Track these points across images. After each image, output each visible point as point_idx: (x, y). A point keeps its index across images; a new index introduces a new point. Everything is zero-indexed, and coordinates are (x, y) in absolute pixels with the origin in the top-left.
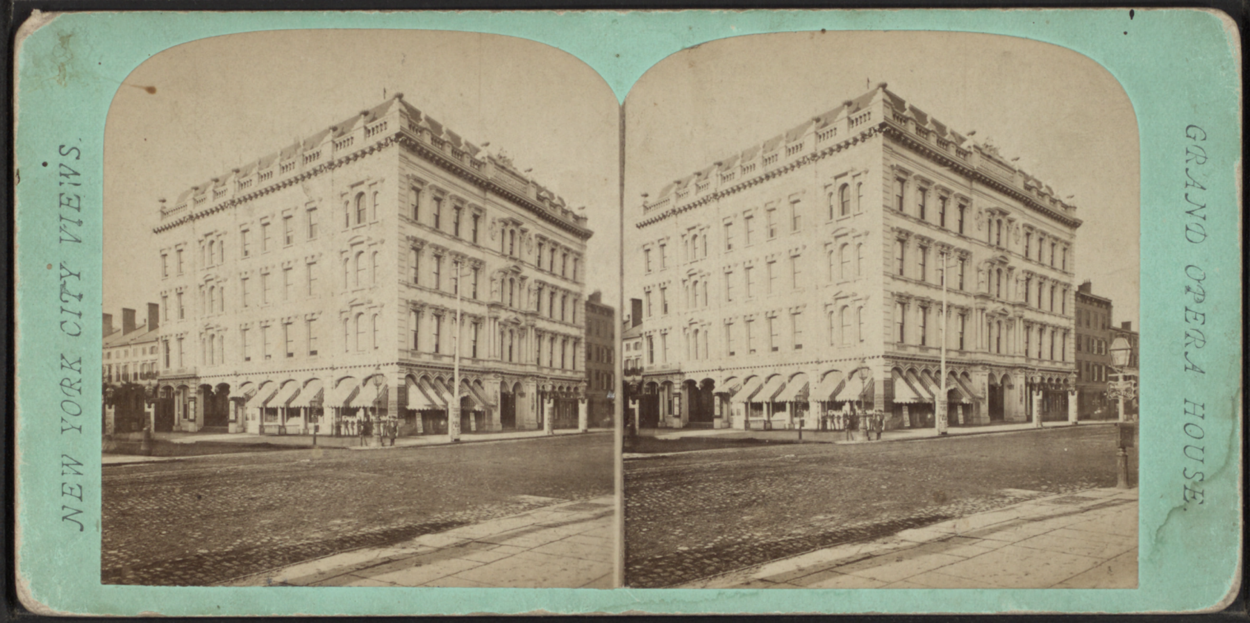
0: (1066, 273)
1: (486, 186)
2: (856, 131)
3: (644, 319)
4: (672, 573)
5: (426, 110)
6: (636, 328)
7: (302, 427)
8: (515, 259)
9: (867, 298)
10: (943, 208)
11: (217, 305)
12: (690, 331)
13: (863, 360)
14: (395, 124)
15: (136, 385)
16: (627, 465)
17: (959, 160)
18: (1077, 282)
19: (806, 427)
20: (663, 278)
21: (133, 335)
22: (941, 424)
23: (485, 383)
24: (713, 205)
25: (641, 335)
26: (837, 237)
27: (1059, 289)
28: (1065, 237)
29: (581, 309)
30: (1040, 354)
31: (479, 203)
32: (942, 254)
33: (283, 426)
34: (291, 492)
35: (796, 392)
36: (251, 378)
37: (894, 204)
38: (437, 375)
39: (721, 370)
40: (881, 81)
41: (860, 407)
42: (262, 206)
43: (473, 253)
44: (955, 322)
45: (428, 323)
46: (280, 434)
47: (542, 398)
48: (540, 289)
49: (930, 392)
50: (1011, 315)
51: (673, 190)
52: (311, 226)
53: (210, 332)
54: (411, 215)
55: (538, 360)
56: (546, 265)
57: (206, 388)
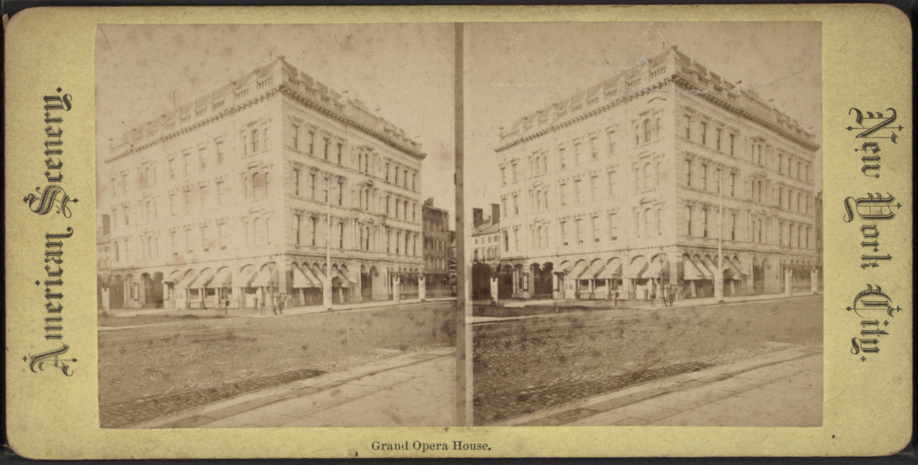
0: (808, 184)
1: (347, 123)
2: (263, 91)
3: (501, 218)
4: (141, 413)
5: (300, 68)
6: (496, 225)
7: (607, 293)
8: (369, 176)
9: (273, 212)
10: (719, 137)
11: (542, 204)
12: (535, 228)
13: (662, 248)
14: (279, 79)
15: (485, 265)
16: (477, 328)
17: (337, 111)
18: (423, 200)
19: (620, 297)
20: (515, 188)
21: (482, 227)
22: (718, 294)
23: (349, 267)
24: (551, 135)
25: (109, 242)
26: (642, 158)
27: (804, 195)
28: (806, 157)
29: (419, 211)
30: (397, 250)
31: (735, 126)
32: (326, 179)
33: (593, 293)
34: (210, 350)
35: (613, 272)
36: (568, 258)
37: (291, 143)
38: (314, 262)
39: (558, 256)
40: (673, 44)
41: (268, 291)
42: (185, 141)
43: (730, 163)
44: (728, 219)
45: (698, 213)
46: (590, 299)
47: (784, 269)
48: (388, 197)
49: (710, 272)
50: (769, 215)
51: (521, 125)
52: (220, 155)
53: (538, 224)
54: (685, 135)
55: (388, 249)
56: (392, 180)
57: (535, 266)
